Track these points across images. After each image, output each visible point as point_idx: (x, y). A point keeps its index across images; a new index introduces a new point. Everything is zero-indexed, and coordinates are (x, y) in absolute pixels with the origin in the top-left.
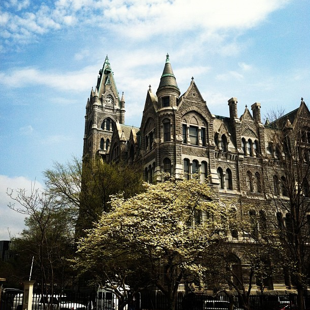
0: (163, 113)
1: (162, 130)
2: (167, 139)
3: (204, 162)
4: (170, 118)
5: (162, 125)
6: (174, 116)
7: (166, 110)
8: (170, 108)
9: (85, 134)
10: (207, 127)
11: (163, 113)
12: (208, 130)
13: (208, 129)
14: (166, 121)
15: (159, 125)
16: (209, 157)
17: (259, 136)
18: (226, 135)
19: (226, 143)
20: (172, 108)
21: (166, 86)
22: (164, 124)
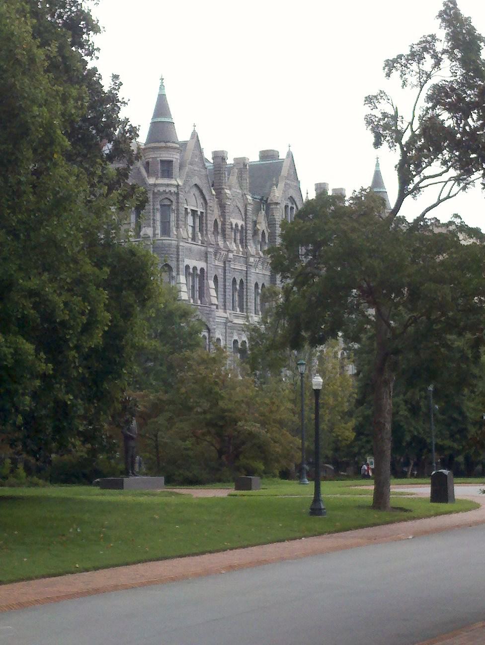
0: (164, 188)
1: (158, 216)
2: (166, 231)
3: (192, 210)
4: (172, 199)
5: (159, 207)
6: (177, 194)
7: (168, 185)
8: (174, 182)
9: (399, 192)
10: (206, 210)
11: (164, 188)
12: (206, 216)
13: (206, 213)
14: (167, 202)
15: (154, 205)
16: (206, 261)
17: (246, 218)
18: (218, 220)
19: (159, 193)
20: (175, 183)
21: (169, 142)
22: (161, 205)
